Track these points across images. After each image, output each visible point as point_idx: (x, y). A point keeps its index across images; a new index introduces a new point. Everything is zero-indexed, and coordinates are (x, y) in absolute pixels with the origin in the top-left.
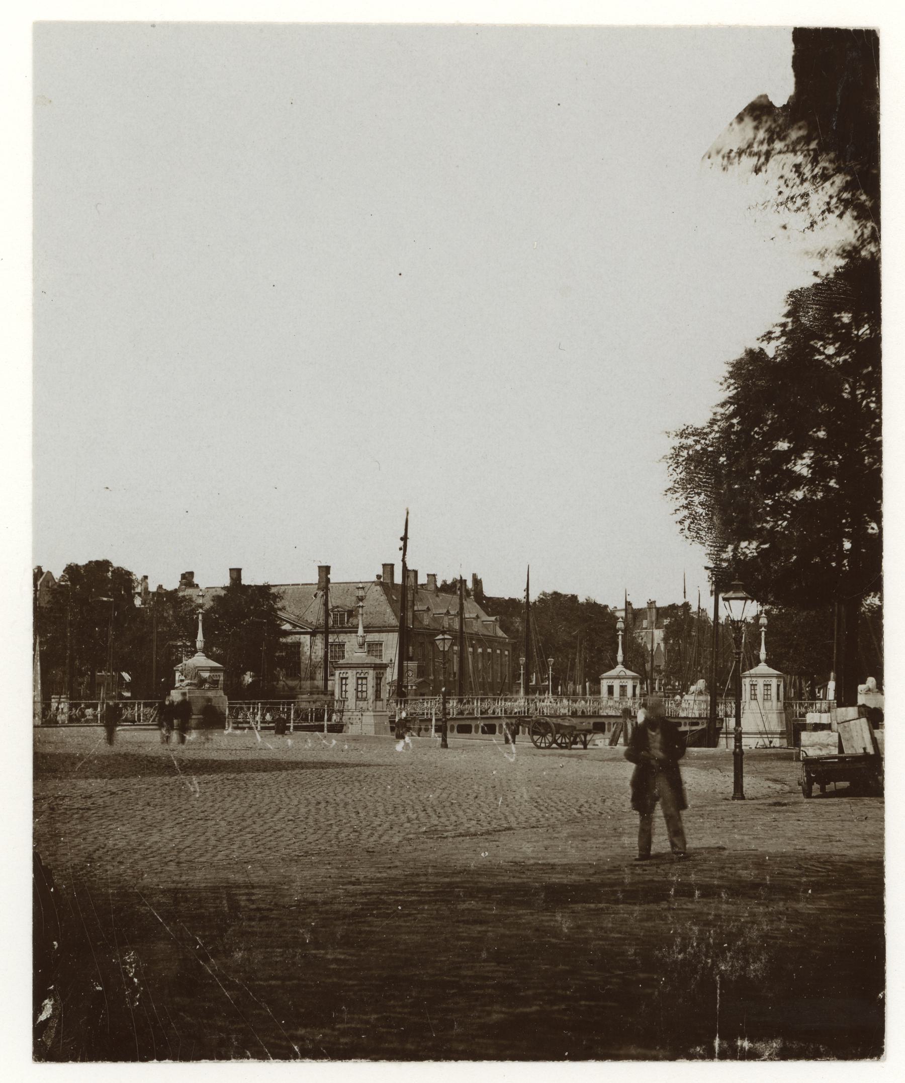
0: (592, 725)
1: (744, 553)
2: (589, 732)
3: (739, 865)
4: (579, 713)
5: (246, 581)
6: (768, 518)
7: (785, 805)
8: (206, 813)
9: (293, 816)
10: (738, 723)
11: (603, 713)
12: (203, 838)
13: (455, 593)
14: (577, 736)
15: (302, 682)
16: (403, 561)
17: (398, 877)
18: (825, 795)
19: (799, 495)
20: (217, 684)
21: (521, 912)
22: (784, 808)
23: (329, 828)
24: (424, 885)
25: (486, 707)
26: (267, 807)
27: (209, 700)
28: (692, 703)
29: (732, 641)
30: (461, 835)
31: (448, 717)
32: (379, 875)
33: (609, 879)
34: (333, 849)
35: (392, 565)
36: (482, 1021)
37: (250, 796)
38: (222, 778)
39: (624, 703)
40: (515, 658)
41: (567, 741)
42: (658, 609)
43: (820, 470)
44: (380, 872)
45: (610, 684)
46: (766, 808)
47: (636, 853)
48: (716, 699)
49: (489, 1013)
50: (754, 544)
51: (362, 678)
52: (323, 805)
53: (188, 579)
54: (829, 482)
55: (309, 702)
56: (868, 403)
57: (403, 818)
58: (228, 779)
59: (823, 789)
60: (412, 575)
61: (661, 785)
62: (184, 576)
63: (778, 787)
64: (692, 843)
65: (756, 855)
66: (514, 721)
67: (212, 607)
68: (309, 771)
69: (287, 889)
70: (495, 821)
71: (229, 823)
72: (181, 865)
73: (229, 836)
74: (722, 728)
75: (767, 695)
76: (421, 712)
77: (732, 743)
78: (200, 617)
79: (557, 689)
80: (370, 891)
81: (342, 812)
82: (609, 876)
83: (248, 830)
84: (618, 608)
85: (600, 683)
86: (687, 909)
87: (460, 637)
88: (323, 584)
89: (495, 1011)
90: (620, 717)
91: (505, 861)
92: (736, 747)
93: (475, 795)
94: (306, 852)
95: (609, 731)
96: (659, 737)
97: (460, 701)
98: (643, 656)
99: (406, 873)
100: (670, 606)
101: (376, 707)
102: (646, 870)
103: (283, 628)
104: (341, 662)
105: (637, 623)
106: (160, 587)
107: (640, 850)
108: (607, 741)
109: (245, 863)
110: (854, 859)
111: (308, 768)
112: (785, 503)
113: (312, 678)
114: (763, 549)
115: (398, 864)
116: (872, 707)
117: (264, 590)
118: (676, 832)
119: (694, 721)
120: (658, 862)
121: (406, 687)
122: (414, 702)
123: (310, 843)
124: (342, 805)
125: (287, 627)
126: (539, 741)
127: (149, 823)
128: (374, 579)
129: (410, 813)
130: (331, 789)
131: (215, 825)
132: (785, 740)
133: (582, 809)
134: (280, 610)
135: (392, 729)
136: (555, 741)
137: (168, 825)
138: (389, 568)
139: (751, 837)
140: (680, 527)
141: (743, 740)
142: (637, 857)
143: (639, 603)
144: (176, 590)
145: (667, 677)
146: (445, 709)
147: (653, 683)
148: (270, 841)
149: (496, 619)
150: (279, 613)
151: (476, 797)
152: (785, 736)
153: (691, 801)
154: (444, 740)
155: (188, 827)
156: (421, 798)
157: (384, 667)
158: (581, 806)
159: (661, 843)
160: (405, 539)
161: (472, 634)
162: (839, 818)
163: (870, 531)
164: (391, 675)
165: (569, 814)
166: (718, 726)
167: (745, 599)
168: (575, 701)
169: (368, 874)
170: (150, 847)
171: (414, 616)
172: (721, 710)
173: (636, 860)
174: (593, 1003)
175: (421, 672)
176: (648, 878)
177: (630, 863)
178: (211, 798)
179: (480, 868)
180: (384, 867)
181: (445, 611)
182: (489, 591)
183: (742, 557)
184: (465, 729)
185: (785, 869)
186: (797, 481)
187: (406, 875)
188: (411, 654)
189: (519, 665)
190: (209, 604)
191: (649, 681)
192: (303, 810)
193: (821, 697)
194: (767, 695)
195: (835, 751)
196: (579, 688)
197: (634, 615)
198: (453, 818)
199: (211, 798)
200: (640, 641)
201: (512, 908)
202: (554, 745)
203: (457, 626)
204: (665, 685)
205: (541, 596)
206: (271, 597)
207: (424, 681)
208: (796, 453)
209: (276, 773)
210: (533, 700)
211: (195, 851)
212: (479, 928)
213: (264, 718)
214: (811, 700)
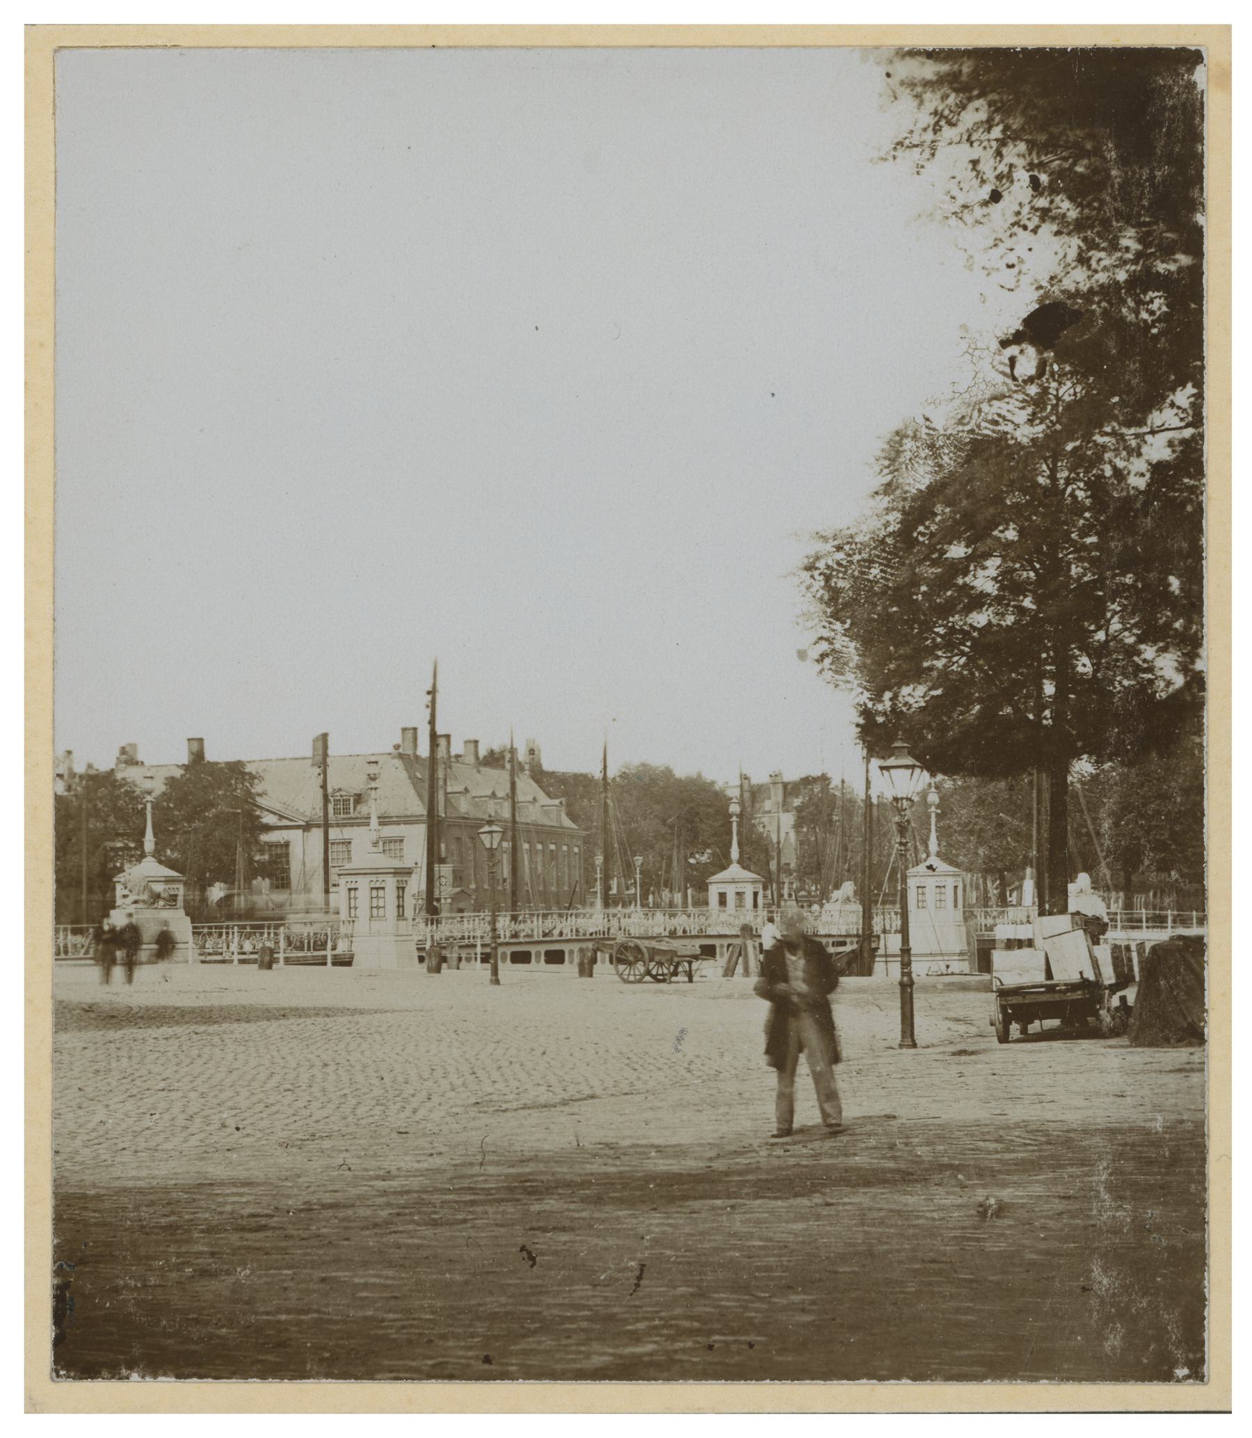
0: (697, 948)
1: (906, 704)
2: (696, 957)
3: (916, 1140)
4: (680, 933)
5: (211, 756)
6: (940, 653)
7: (972, 1053)
8: (169, 1081)
9: (292, 1084)
10: (905, 940)
11: (711, 932)
12: (167, 1116)
13: (503, 767)
14: (678, 964)
15: (294, 896)
16: (432, 722)
17: (443, 1168)
18: (1027, 1038)
19: (980, 619)
20: (175, 901)
21: (620, 1213)
22: (973, 1057)
23: (343, 1101)
24: (482, 1178)
25: (551, 926)
26: (254, 1072)
27: (166, 923)
28: (836, 914)
29: (894, 827)
30: (525, 1107)
31: (499, 941)
32: (416, 1166)
33: (738, 1164)
34: (350, 1130)
35: (415, 729)
36: (578, 1366)
37: (230, 1057)
38: (187, 1031)
39: (742, 917)
40: (588, 859)
41: (666, 971)
42: (785, 785)
43: (1010, 586)
44: (419, 1162)
45: (722, 891)
46: (948, 1058)
47: (773, 1127)
48: (870, 910)
49: (588, 1356)
50: (921, 689)
51: (377, 889)
52: (333, 1067)
53: (128, 757)
54: (1022, 601)
55: (305, 924)
56: (1073, 490)
57: (445, 1084)
58: (196, 1033)
59: (1024, 1031)
60: (443, 742)
61: (807, 1028)
62: (123, 751)
63: (962, 1028)
64: (851, 1110)
65: (939, 1125)
66: (590, 945)
67: (164, 794)
68: (309, 1021)
69: (291, 1187)
70: (573, 1086)
71: (203, 1095)
72: (139, 1154)
73: (204, 1113)
74: (878, 948)
75: (940, 900)
76: (459, 935)
77: (895, 969)
78: (149, 806)
79: (647, 899)
80: (407, 1188)
81: (360, 1078)
82: (737, 1160)
83: (230, 1104)
84: (730, 784)
85: (707, 890)
86: (850, 1203)
87: (513, 830)
88: (319, 758)
89: (595, 1353)
90: (737, 936)
91: (591, 1143)
92: (903, 974)
93: (542, 1050)
94: (313, 1135)
95: (722, 955)
96: (802, 962)
97: (514, 918)
98: (766, 851)
99: (454, 1162)
100: (802, 779)
101: (397, 930)
102: (788, 1151)
103: (264, 820)
104: (348, 866)
105: (757, 805)
106: (90, 766)
107: (779, 1122)
108: (720, 971)
109: (228, 1150)
110: (1075, 1126)
111: (308, 1016)
112: (962, 631)
113: (307, 889)
114: (933, 697)
115: (443, 1149)
116: (1090, 915)
117: (236, 769)
118: (828, 1095)
119: (841, 939)
120: (805, 1138)
121: (438, 900)
122: (450, 921)
123: (317, 1121)
124: (359, 1067)
125: (269, 819)
126: (627, 972)
127: (90, 1096)
128: (390, 749)
129: (453, 1077)
130: (342, 1045)
131: (182, 1097)
132: (966, 963)
133: (691, 1067)
134: (260, 795)
135: (421, 959)
136: (648, 973)
137: (116, 1099)
138: (410, 734)
139: (930, 1099)
140: (818, 667)
141: (914, 965)
142: (775, 1133)
143: (759, 777)
144: (113, 770)
145: (800, 880)
146: (494, 930)
147: (780, 889)
148: (262, 1119)
149: (561, 803)
150: (258, 799)
151: (544, 1053)
152: (966, 957)
153: (846, 1051)
154: (495, 971)
155: (145, 1100)
156: (468, 1056)
157: (408, 872)
158: (691, 1063)
159: (807, 1112)
160: (432, 693)
161: (528, 824)
162: (1050, 1070)
163: (1080, 669)
164: (417, 884)
165: (674, 1074)
166: (874, 945)
167: (913, 767)
168: (673, 915)
169: (402, 1164)
170: (94, 1130)
171: (447, 800)
172: (877, 924)
173: (773, 1136)
174: (731, 1338)
175: (458, 878)
176: (792, 1161)
177: (765, 1141)
178: (175, 1060)
179: (557, 1153)
180: (424, 1154)
181: (489, 793)
182: (547, 766)
183: (904, 709)
184: (521, 958)
185: (981, 1144)
186: (978, 601)
187: (456, 1165)
188: (443, 855)
189: (593, 866)
190: (159, 787)
191: (774, 886)
192: (305, 1077)
193: (1014, 903)
194: (940, 900)
195: (1040, 978)
196: (678, 897)
197: (754, 794)
198: (515, 1084)
199: (175, 1060)
200: (761, 829)
201: (607, 1208)
202: (648, 978)
203: (506, 814)
204: (797, 891)
205: (623, 770)
206: (247, 777)
207: (462, 891)
208: (977, 559)
209: (264, 1024)
210: (614, 915)
211: (156, 1134)
212: (564, 1237)
213: (242, 947)
214: (1001, 907)
